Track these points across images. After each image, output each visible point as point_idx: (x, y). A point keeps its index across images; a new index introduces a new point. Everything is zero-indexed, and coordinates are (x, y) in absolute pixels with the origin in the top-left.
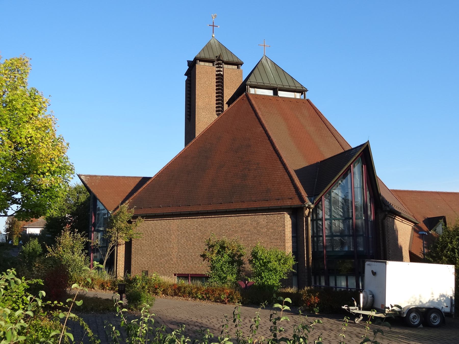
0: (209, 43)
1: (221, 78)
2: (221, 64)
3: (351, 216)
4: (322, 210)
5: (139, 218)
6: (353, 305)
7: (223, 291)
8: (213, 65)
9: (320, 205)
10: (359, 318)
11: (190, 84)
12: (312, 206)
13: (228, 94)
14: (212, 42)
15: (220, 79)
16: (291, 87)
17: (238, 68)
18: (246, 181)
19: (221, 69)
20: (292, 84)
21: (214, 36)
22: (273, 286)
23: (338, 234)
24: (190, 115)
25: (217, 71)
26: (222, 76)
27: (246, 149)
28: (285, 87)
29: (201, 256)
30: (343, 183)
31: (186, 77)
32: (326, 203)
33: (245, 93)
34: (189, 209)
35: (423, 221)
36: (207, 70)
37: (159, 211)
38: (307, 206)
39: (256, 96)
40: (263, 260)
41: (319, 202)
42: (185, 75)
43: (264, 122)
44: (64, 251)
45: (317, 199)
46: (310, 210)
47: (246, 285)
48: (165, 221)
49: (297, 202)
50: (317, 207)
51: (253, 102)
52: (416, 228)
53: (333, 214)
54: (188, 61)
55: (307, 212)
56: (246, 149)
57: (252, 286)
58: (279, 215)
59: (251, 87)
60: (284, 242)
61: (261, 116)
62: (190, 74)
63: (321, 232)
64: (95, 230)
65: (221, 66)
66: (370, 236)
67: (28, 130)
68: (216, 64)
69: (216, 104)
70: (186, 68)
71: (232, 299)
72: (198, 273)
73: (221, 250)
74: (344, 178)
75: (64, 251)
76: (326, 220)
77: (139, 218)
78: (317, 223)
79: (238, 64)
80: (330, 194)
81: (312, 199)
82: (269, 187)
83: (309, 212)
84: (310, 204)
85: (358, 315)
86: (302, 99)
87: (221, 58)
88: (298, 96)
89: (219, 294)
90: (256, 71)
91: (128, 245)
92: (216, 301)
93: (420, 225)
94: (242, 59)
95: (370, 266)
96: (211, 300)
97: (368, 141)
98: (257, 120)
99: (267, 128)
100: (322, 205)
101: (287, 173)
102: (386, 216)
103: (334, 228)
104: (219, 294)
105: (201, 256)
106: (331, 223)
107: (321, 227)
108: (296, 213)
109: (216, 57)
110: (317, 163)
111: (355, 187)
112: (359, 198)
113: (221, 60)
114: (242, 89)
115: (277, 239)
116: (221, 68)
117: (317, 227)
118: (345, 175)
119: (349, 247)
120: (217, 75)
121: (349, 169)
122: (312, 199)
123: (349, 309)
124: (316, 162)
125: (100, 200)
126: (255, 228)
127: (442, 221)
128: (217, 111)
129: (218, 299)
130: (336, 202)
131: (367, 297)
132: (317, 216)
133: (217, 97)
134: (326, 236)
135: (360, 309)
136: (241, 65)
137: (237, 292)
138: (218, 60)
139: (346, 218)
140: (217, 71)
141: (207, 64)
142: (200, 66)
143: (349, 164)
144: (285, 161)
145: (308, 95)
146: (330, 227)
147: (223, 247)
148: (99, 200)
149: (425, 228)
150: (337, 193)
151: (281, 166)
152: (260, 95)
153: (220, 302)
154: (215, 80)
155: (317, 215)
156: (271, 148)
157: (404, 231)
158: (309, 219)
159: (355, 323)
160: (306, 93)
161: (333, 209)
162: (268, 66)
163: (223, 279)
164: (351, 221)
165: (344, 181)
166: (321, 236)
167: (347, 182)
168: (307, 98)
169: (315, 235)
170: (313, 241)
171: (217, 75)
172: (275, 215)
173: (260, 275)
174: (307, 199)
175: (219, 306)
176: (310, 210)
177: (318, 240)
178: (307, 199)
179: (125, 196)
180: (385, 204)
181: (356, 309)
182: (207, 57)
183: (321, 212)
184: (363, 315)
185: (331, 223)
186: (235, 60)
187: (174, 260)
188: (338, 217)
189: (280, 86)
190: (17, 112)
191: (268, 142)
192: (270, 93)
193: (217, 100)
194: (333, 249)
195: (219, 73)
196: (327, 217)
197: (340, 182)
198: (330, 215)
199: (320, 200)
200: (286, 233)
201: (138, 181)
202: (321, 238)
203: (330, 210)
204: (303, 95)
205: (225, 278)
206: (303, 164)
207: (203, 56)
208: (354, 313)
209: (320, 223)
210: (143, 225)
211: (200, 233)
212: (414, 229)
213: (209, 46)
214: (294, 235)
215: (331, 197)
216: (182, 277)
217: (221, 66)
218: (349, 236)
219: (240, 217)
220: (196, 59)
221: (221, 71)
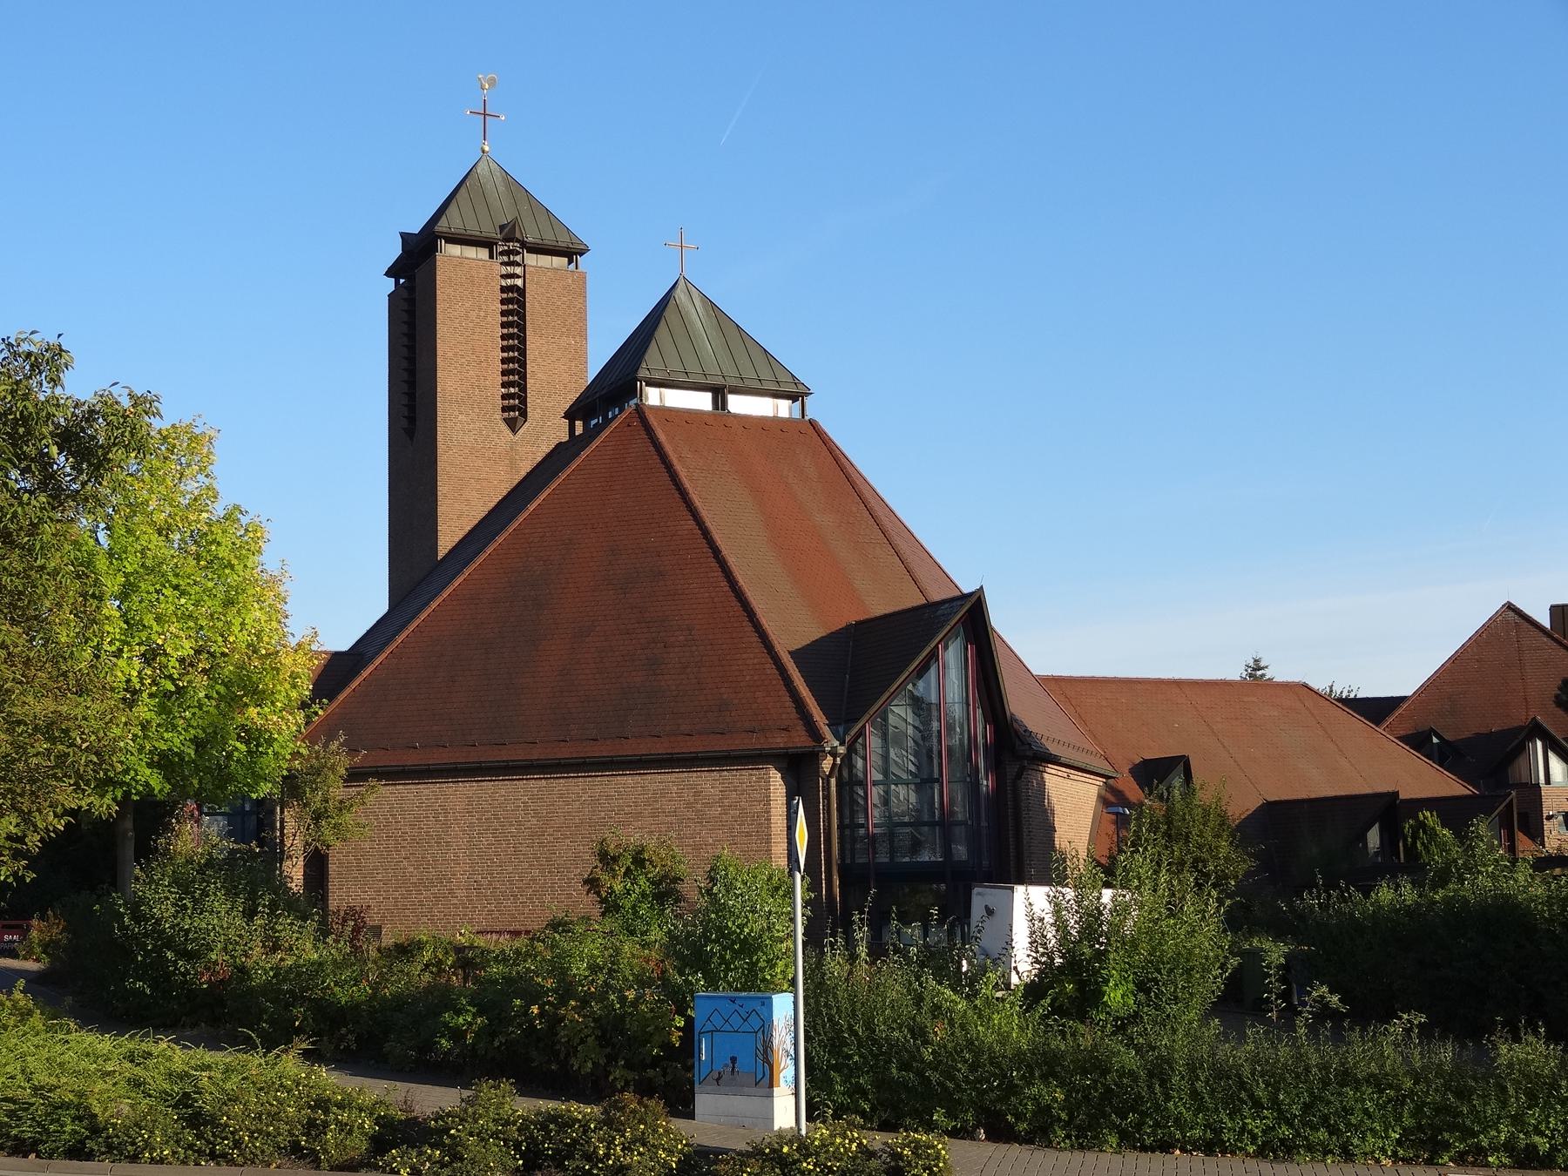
3: (936, 776)
4: (865, 759)
8: (491, 257)
9: (859, 747)
11: (411, 313)
12: (842, 750)
13: (557, 381)
15: (514, 302)
17: (570, 262)
19: (518, 270)
20: (766, 374)
24: (412, 419)
25: (504, 277)
26: (521, 292)
29: (586, 882)
31: (390, 285)
32: (874, 742)
34: (504, 755)
35: (1131, 771)
36: (474, 273)
37: (411, 759)
39: (671, 415)
42: (388, 274)
50: (851, 749)
51: (662, 437)
53: (894, 769)
54: (403, 235)
55: (827, 764)
59: (651, 383)
60: (768, 842)
61: (687, 484)
65: (518, 258)
66: (984, 824)
68: (502, 253)
70: (395, 251)
76: (875, 783)
78: (852, 792)
79: (572, 252)
80: (885, 719)
81: (841, 729)
83: (834, 764)
84: (836, 743)
87: (518, 235)
88: (784, 408)
90: (662, 333)
93: (1120, 786)
95: (981, 896)
99: (708, 524)
100: (864, 746)
102: (1022, 770)
105: (586, 882)
106: (887, 792)
107: (861, 802)
108: (799, 770)
109: (502, 227)
111: (949, 700)
115: (748, 834)
116: (518, 265)
117: (853, 802)
118: (922, 671)
120: (503, 289)
121: (933, 655)
122: (841, 729)
126: (689, 805)
127: (1181, 767)
128: (504, 409)
130: (899, 740)
132: (850, 772)
133: (503, 361)
138: (507, 240)
139: (924, 781)
140: (504, 277)
141: (471, 252)
144: (763, 621)
145: (815, 409)
146: (886, 801)
147: (639, 861)
150: (900, 714)
151: (755, 638)
155: (851, 766)
157: (1072, 804)
158: (833, 781)
161: (892, 755)
164: (936, 787)
165: (921, 684)
166: (862, 826)
170: (841, 837)
182: (473, 229)
183: (859, 763)
185: (887, 792)
186: (563, 241)
187: (459, 893)
188: (904, 776)
192: (701, 401)
193: (504, 373)
194: (892, 858)
195: (509, 282)
197: (910, 687)
198: (886, 772)
199: (861, 733)
203: (885, 757)
209: (861, 792)
212: (1103, 801)
215: (886, 726)
217: (518, 258)
218: (932, 824)
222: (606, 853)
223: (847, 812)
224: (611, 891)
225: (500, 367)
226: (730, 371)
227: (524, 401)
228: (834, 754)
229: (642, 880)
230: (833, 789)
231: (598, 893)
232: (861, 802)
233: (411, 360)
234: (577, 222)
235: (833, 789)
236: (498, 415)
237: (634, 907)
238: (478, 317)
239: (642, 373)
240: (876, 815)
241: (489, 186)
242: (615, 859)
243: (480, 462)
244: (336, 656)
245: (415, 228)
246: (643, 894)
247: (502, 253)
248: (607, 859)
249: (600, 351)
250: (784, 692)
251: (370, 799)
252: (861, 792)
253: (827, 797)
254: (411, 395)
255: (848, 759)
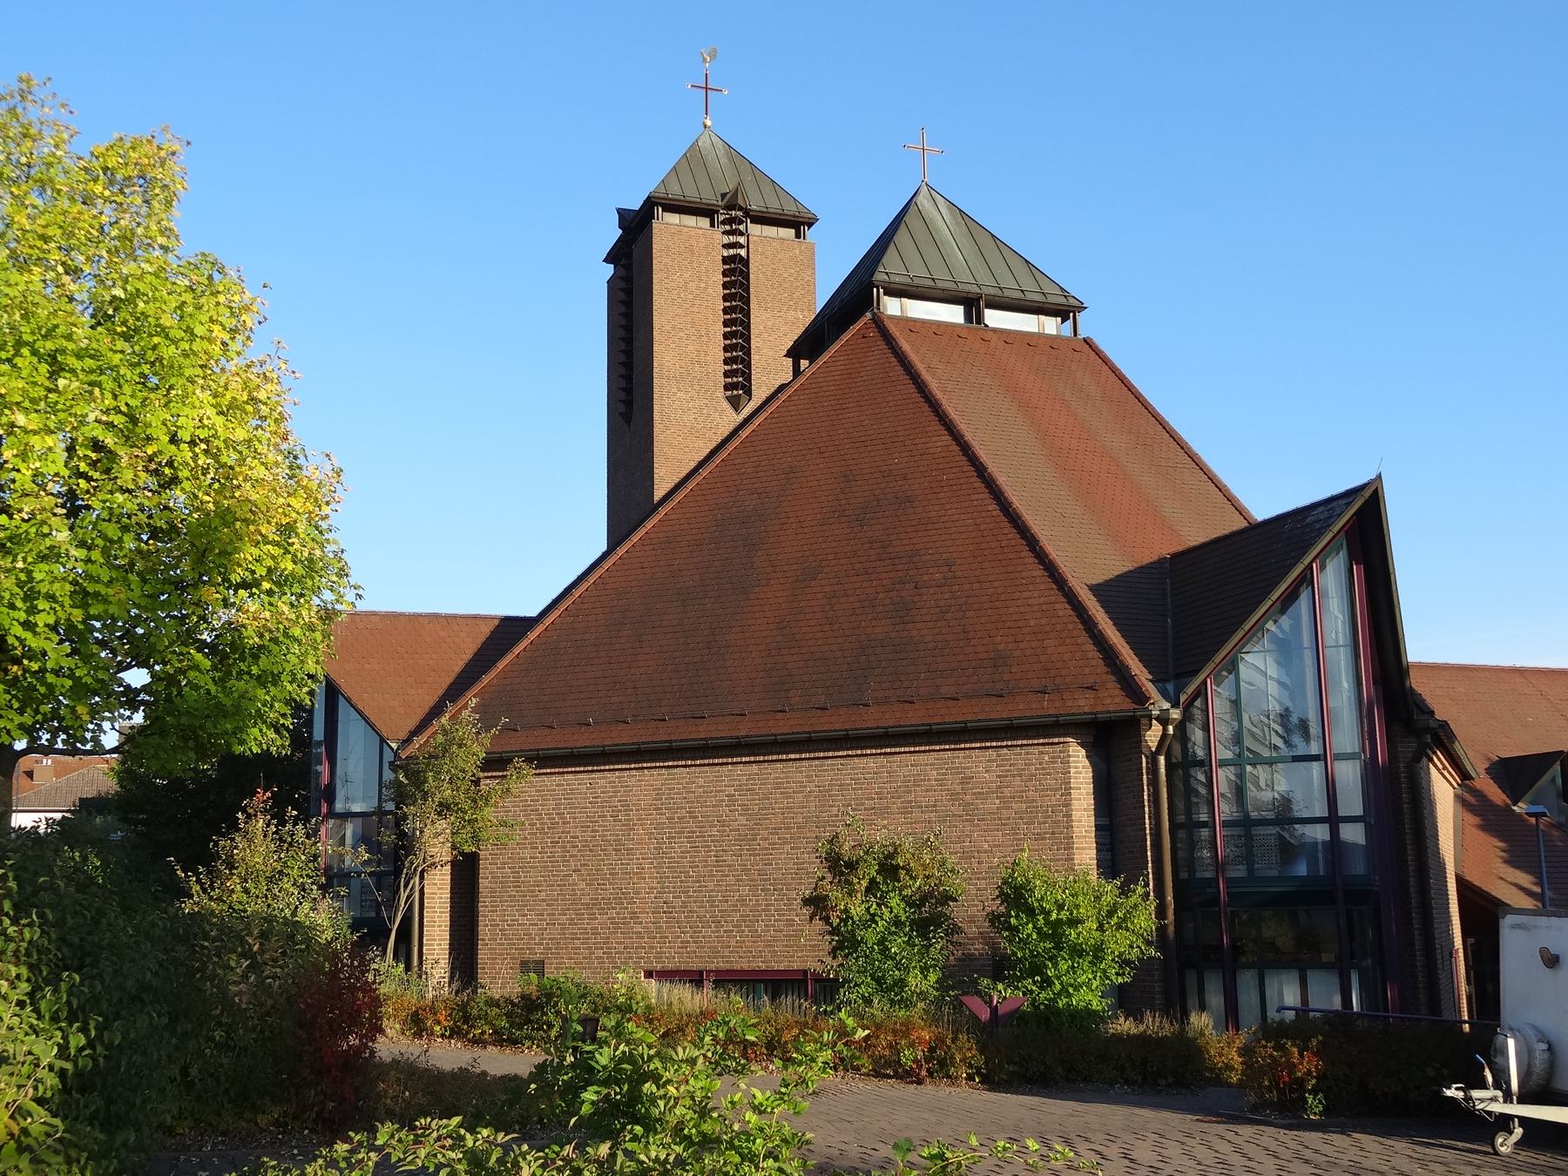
0: (695, 146)
1: (742, 272)
2: (741, 222)
4: (1206, 728)
5: (518, 762)
6: (1483, 1085)
7: (906, 1034)
8: (712, 225)
9: (1197, 714)
10: (1511, 1133)
11: (628, 292)
13: (775, 331)
14: (704, 143)
15: (737, 273)
16: (1030, 296)
17: (798, 236)
18: (910, 626)
19: (742, 240)
20: (1028, 284)
21: (709, 123)
22: (1089, 1014)
23: (1270, 815)
24: (629, 403)
26: (745, 262)
27: (844, 515)
28: (1007, 293)
29: (807, 902)
30: (1282, 630)
32: (1219, 705)
33: (868, 315)
36: (693, 242)
37: (583, 740)
38: (1155, 713)
40: (1048, 913)
41: (1195, 699)
42: (607, 260)
43: (953, 414)
44: (246, 891)
45: (1191, 689)
46: (1165, 730)
47: (994, 1010)
48: (608, 775)
49: (1117, 700)
50: (1187, 717)
51: (905, 346)
52: (1467, 796)
53: (1248, 742)
54: (620, 212)
55: (1153, 736)
56: (844, 515)
57: (1017, 1015)
58: (1047, 749)
60: (1069, 847)
61: (939, 395)
62: (629, 256)
63: (1204, 809)
64: (331, 814)
65: (742, 227)
67: (198, 412)
68: (723, 222)
69: (726, 362)
71: (943, 1064)
72: (737, 967)
73: (879, 879)
74: (1283, 611)
75: (246, 891)
76: (1223, 764)
77: (518, 762)
78: (1187, 777)
79: (799, 223)
81: (1170, 687)
82: (1001, 647)
83: (1164, 735)
84: (1166, 705)
85: (1504, 1122)
86: (1067, 339)
87: (740, 202)
88: (1051, 325)
89: (890, 1046)
90: (902, 237)
91: (465, 872)
92: (878, 1074)
94: (808, 199)
96: (857, 1069)
97: (1379, 476)
98: (926, 408)
99: (968, 437)
101: (1065, 596)
103: (1251, 792)
104: (890, 1046)
105: (807, 902)
106: (1241, 776)
107: (1203, 791)
108: (1110, 741)
109: (723, 196)
110: (1161, 561)
111: (1329, 641)
112: (1345, 685)
113: (741, 209)
114: (856, 297)
116: (741, 234)
117: (1190, 791)
119: (1312, 864)
120: (725, 260)
121: (1306, 579)
122: (1170, 687)
123: (1468, 1099)
124: (1155, 558)
125: (354, 700)
126: (954, 796)
128: (727, 387)
129: (888, 1064)
131: (1530, 1051)
133: (726, 336)
134: (1225, 824)
135: (1508, 1097)
136: (810, 225)
137: (963, 1037)
138: (729, 207)
141: (690, 220)
142: (666, 224)
143: (1306, 562)
145: (1088, 325)
146: (1239, 791)
147: (890, 869)
148: (349, 700)
149: (1496, 794)
151: (1038, 571)
152: (924, 322)
153: (897, 1076)
154: (720, 279)
156: (993, 507)
158: (1162, 759)
159: (1496, 1153)
160: (1080, 317)
162: (942, 221)
163: (893, 990)
165: (1285, 621)
166: (1204, 824)
167: (1296, 627)
168: (1082, 334)
169: (1181, 818)
171: (725, 260)
172: (1031, 749)
173: (1036, 969)
174: (1151, 689)
175: (891, 1089)
176: (1165, 730)
177: (1192, 845)
178: (1151, 689)
179: (445, 687)
180: (1418, 707)
181: (1494, 1099)
182: (691, 194)
183: (1197, 735)
184: (1524, 1121)
185: (1241, 776)
186: (790, 209)
187: (643, 918)
188: (1266, 753)
189: (991, 291)
190: (156, 340)
191: (979, 484)
192: (953, 314)
193: (726, 349)
194: (1250, 870)
195: (732, 252)
196: (1228, 755)
199: (1201, 692)
200: (1076, 815)
201: (486, 630)
202: (1205, 833)
204: (1070, 323)
205: (901, 984)
206: (1113, 565)
207: (675, 191)
208: (1489, 1113)
210: (532, 789)
211: (743, 820)
213: (693, 159)
214: (1105, 821)
216: (735, 982)
217: (742, 227)
219: (897, 758)
220: (650, 204)
221: (742, 247)
222: (839, 857)
223: (1181, 805)
224: (846, 917)
225: (722, 343)
226: (985, 278)
227: (748, 378)
228: (1164, 720)
229: (894, 901)
230: (1163, 770)
231: (826, 920)
232: (1203, 791)
233: (629, 341)
234: (806, 194)
235: (1163, 770)
236: (720, 393)
237: (881, 942)
238: (698, 288)
239: (879, 276)
240: (1225, 810)
241: (711, 158)
242: (852, 866)
243: (691, 418)
244: (508, 621)
245: (635, 204)
246: (897, 923)
247: (723, 222)
248: (840, 866)
249: (827, 283)
250: (1084, 638)
251: (514, 786)
252: (1202, 778)
253: (1154, 782)
254: (628, 378)
255: (1181, 727)
